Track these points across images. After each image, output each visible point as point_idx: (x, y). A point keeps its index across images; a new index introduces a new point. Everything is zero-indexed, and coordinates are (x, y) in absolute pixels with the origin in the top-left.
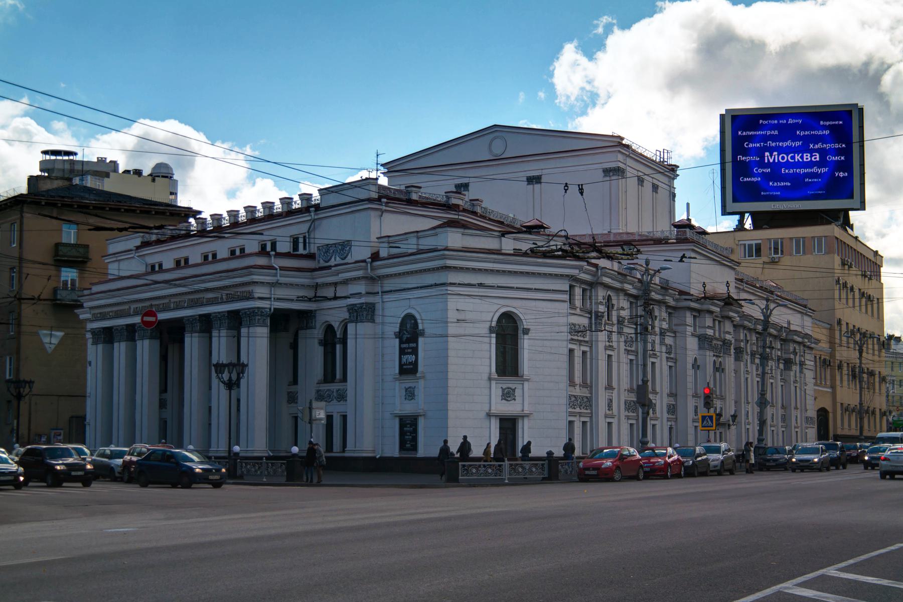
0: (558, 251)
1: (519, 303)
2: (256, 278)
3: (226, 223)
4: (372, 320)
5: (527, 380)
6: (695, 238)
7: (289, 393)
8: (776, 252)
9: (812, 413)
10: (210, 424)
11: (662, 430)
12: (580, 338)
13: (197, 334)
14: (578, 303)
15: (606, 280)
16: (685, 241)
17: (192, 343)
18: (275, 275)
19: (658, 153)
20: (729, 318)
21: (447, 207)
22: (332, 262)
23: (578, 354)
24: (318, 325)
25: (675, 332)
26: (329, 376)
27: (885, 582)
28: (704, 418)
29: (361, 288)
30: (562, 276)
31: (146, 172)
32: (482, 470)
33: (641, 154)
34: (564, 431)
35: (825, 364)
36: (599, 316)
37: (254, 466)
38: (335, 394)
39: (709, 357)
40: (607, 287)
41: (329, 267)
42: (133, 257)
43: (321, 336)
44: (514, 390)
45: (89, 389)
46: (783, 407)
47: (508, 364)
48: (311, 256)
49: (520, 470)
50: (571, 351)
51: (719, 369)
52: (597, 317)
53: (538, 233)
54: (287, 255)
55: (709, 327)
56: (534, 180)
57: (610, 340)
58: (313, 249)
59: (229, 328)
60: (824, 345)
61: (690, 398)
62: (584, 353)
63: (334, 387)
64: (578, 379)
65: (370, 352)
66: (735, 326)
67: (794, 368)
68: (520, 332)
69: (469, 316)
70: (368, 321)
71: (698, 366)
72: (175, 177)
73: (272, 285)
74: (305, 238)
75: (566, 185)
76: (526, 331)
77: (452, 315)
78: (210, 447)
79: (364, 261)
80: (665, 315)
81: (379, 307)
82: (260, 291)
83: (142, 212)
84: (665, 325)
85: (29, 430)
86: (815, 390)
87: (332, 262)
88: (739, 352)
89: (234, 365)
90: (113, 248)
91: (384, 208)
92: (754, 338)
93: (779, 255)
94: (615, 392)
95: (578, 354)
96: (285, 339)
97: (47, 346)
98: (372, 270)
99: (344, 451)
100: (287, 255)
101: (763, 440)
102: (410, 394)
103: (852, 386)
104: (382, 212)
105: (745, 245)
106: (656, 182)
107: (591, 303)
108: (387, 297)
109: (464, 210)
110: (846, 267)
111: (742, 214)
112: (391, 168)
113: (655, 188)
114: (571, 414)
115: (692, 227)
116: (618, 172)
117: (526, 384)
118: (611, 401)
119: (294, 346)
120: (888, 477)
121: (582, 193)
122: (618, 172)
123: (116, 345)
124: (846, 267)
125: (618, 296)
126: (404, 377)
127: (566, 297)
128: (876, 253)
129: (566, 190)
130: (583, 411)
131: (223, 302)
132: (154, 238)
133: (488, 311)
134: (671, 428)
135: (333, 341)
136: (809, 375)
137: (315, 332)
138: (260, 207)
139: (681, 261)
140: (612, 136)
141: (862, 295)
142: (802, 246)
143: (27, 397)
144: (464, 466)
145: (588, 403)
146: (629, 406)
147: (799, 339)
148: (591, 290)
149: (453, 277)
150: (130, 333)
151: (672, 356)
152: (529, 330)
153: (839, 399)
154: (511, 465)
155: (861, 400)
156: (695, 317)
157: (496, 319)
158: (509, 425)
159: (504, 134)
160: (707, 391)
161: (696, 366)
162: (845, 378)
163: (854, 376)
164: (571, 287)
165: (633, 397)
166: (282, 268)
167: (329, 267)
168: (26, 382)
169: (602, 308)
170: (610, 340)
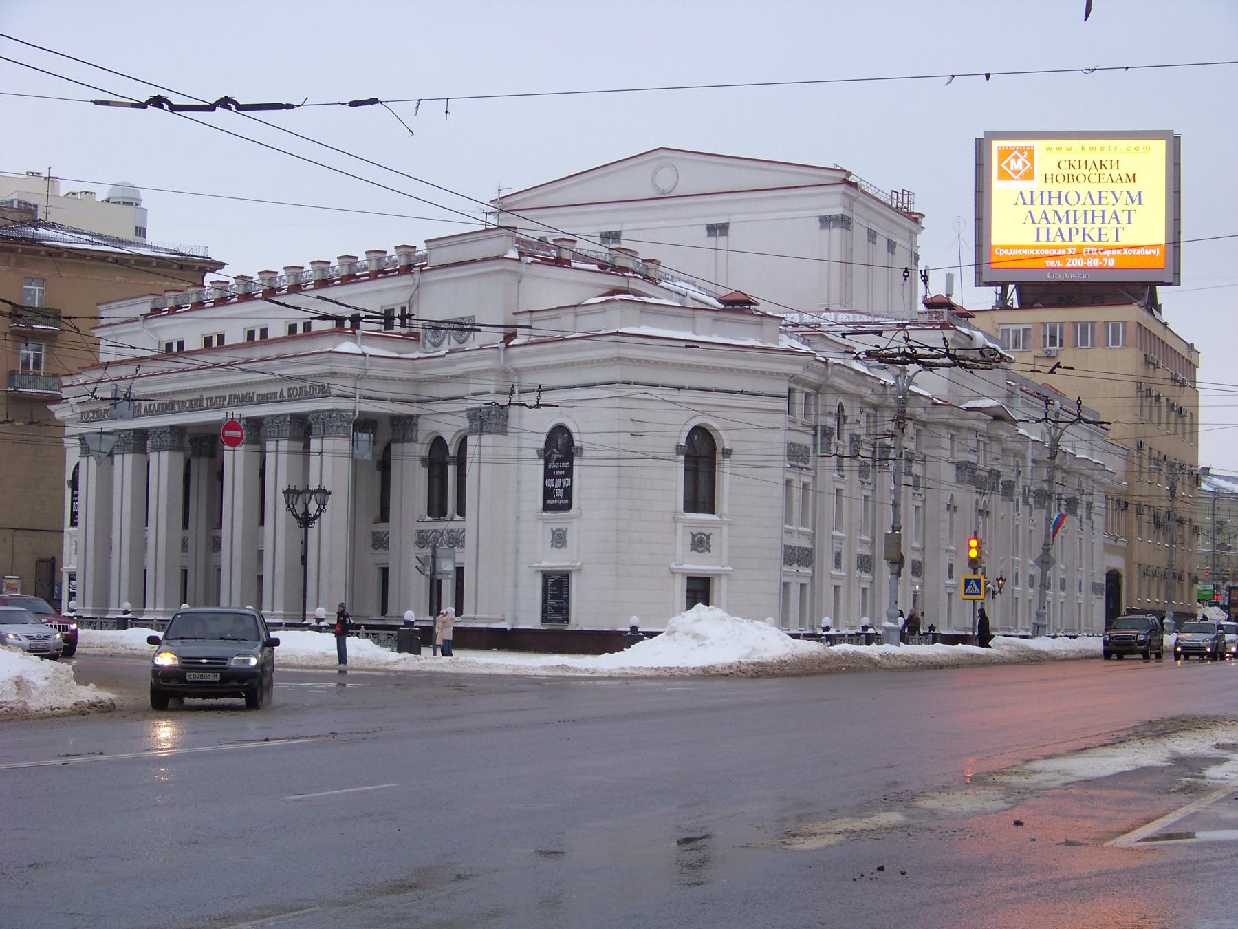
0: (899, 355)
7: (374, 534)
8: (1053, 343)
14: (799, 417)
15: (839, 382)
17: (236, 462)
19: (895, 195)
23: (797, 484)
24: (421, 437)
33: (872, 197)
36: (827, 433)
38: (445, 537)
39: (967, 497)
42: (140, 331)
44: (708, 537)
47: (700, 495)
50: (788, 483)
51: (983, 512)
53: (741, 312)
59: (292, 438)
62: (805, 485)
63: (442, 525)
65: (503, 478)
68: (719, 457)
69: (648, 427)
70: (497, 433)
72: (143, 205)
90: (110, 313)
98: (505, 360)
101: (1043, 615)
102: (559, 539)
111: (1004, 286)
113: (891, 246)
115: (951, 306)
120: (1114, 656)
128: (1190, 346)
129: (906, 277)
135: (444, 463)
136: (1098, 521)
139: (1052, 372)
141: (1172, 406)
148: (816, 396)
150: (139, 441)
152: (731, 451)
157: (685, 435)
163: (1157, 525)
164: (790, 390)
169: (831, 422)
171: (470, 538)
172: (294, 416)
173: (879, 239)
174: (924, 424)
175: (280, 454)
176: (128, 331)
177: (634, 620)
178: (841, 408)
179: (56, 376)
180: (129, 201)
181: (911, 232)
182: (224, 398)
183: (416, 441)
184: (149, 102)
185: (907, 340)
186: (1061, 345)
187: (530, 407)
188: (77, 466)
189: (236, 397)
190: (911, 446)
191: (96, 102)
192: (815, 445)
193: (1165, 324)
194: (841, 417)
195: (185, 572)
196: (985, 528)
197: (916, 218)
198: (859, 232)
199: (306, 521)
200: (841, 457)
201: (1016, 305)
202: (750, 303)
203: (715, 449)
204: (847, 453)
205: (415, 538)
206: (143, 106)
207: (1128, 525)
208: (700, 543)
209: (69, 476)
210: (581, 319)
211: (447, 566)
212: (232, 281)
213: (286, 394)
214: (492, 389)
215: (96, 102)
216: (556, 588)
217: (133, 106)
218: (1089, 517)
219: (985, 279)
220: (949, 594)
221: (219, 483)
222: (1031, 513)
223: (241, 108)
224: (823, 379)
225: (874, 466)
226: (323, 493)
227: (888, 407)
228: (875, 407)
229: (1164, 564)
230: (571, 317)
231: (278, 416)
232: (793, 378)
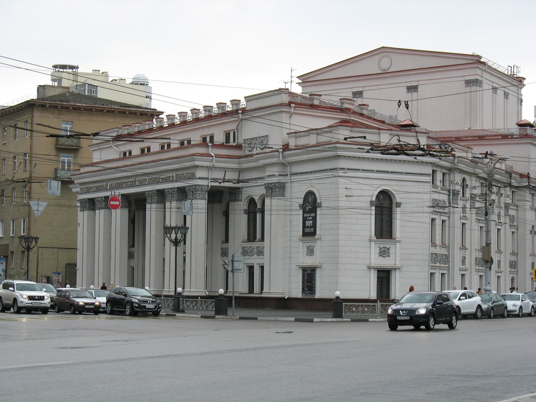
2: (197, 163)
3: (177, 121)
4: (283, 195)
5: (399, 242)
7: (222, 249)
10: (164, 271)
11: (505, 280)
15: (462, 166)
16: (527, 136)
17: (152, 211)
18: (212, 161)
19: (510, 68)
21: (342, 110)
22: (254, 152)
23: (438, 222)
25: (517, 206)
26: (251, 237)
27: (234, 301)
29: (275, 170)
32: (360, 309)
33: (495, 69)
36: (455, 194)
37: (192, 303)
38: (255, 250)
41: (252, 156)
43: (246, 207)
44: (389, 249)
45: (79, 245)
47: (384, 229)
48: (239, 147)
50: (433, 220)
52: (454, 194)
53: (410, 131)
54: (221, 146)
56: (412, 89)
58: (241, 141)
61: (528, 256)
62: (443, 221)
64: (438, 241)
65: (282, 219)
68: (394, 205)
69: (354, 193)
70: (280, 195)
72: (150, 85)
73: (209, 168)
74: (234, 132)
76: (398, 205)
77: (343, 192)
78: (164, 288)
79: (277, 151)
81: (288, 186)
83: (119, 112)
84: (509, 201)
85: (37, 273)
87: (254, 152)
89: (179, 228)
94: (468, 251)
95: (438, 222)
96: (219, 208)
97: (36, 212)
98: (283, 158)
99: (262, 293)
100: (221, 146)
102: (310, 251)
104: (291, 114)
106: (507, 91)
108: (294, 178)
109: (354, 113)
112: (248, 99)
113: (506, 95)
114: (433, 267)
116: (476, 82)
117: (398, 244)
118: (464, 258)
119: (226, 215)
121: (407, 108)
122: (476, 82)
123: (97, 211)
126: (306, 238)
127: (429, 179)
129: (399, 106)
130: (480, 268)
134: (513, 279)
135: (254, 210)
137: (242, 203)
138: (229, 103)
143: (35, 249)
144: (346, 306)
145: (446, 259)
146: (478, 262)
148: (449, 174)
149: (342, 164)
151: (515, 224)
152: (401, 203)
154: (382, 305)
158: (384, 277)
159: (390, 54)
165: (480, 255)
166: (217, 156)
167: (252, 156)
168: (33, 238)
169: (458, 188)
171: (266, 251)
177: (338, 293)
178: (464, 180)
183: (241, 201)
185: (399, 141)
192: (449, 199)
194: (464, 186)
197: (520, 81)
202: (415, 126)
208: (384, 253)
214: (277, 174)
216: (309, 276)
231: (171, 189)
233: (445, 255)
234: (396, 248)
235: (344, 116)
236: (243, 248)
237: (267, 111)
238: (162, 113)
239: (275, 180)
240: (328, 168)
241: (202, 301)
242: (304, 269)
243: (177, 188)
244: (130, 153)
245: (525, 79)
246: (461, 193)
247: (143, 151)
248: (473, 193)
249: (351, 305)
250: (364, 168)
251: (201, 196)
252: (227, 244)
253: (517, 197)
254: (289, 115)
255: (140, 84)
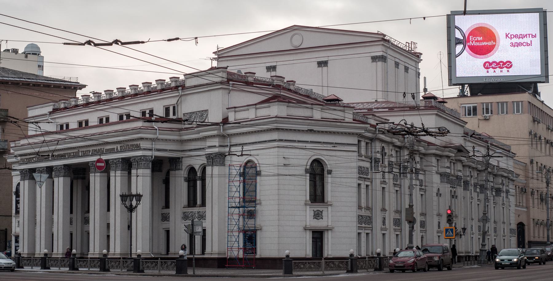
1: (325, 153)
5: (331, 205)
6: (438, 105)
7: (162, 214)
8: (487, 113)
9: (514, 226)
12: (365, 176)
13: (99, 174)
14: (363, 152)
15: (382, 136)
17: (96, 181)
19: (407, 45)
20: (460, 161)
23: (363, 187)
24: (184, 168)
26: (192, 203)
28: (447, 230)
29: (216, 142)
30: (353, 134)
31: (20, 52)
32: (308, 266)
33: (396, 46)
34: (355, 240)
35: (523, 190)
36: (377, 161)
38: (197, 215)
39: (446, 189)
40: (382, 141)
44: (322, 212)
46: (495, 222)
47: (317, 196)
48: (179, 121)
49: (332, 266)
50: (359, 185)
51: (454, 196)
53: (335, 105)
55: (448, 167)
56: (322, 64)
57: (384, 177)
58: (180, 115)
60: (522, 178)
61: (435, 216)
62: (367, 186)
63: (195, 210)
65: (221, 186)
66: (464, 166)
67: (502, 195)
68: (326, 172)
69: (291, 162)
71: (440, 194)
72: (42, 54)
74: (174, 108)
75: (404, 93)
80: (394, 153)
82: (143, 144)
86: (516, 210)
88: (466, 183)
90: (32, 113)
91: (231, 88)
92: (476, 175)
93: (490, 114)
94: (387, 212)
98: (223, 130)
99: (168, 254)
101: (485, 245)
103: (540, 206)
105: (465, 107)
106: (407, 65)
107: (372, 152)
109: (284, 89)
110: (536, 122)
111: (463, 85)
112: (188, 76)
113: (406, 69)
114: (360, 228)
118: (384, 218)
124: (536, 122)
125: (389, 146)
129: (404, 97)
131: (118, 152)
132: (62, 106)
133: (302, 159)
134: (422, 237)
135: (196, 178)
136: (512, 199)
137: (182, 172)
140: (377, 34)
142: (503, 108)
144: (295, 263)
147: (506, 175)
148: (371, 143)
151: (423, 187)
152: (331, 171)
153: (532, 217)
154: (326, 262)
155: (274, 176)
156: (438, 160)
157: (309, 164)
158: (318, 236)
160: (449, 212)
161: (439, 194)
162: (536, 201)
163: (542, 200)
164: (359, 141)
169: (379, 156)
170: (384, 177)
172: (123, 159)
173: (400, 66)
174: (425, 155)
175: (117, 178)
176: (41, 121)
179: (6, 141)
180: (33, 52)
181: (416, 61)
182: (90, 151)
183: (182, 170)
184: (85, 43)
186: (492, 113)
187: (239, 156)
188: (19, 184)
189: (95, 150)
190: (418, 166)
191: (64, 44)
192: (371, 167)
193: (542, 102)
194: (383, 154)
195: (71, 234)
196: (455, 204)
197: (418, 56)
198: (391, 63)
199: (131, 209)
200: (384, 172)
201: (469, 95)
203: (324, 170)
204: (387, 170)
205: (182, 216)
206: (84, 44)
207: (527, 200)
209: (14, 190)
210: (258, 111)
211: (199, 229)
212: (92, 95)
213: (119, 149)
214: (217, 145)
215: (64, 44)
217: (79, 44)
218: (507, 197)
219: (453, 83)
220: (439, 236)
221: (87, 192)
222: (478, 196)
223: (123, 44)
224: (374, 135)
225: (400, 176)
226: (139, 197)
227: (406, 147)
228: (400, 148)
229: (545, 219)
230: (254, 110)
232: (360, 135)
233: (369, 217)
234: (328, 211)
235: (277, 92)
236: (184, 213)
237: (207, 87)
238: (83, 86)
239: (216, 150)
240: (267, 140)
241: (162, 262)
242: (245, 232)
243: (122, 158)
244: (67, 126)
245: (422, 54)
246: (381, 160)
247: (80, 124)
248: (391, 160)
249: (300, 263)
250: (299, 140)
251: (146, 165)
252: (167, 210)
253: (425, 163)
254: (227, 91)
255: (33, 54)
